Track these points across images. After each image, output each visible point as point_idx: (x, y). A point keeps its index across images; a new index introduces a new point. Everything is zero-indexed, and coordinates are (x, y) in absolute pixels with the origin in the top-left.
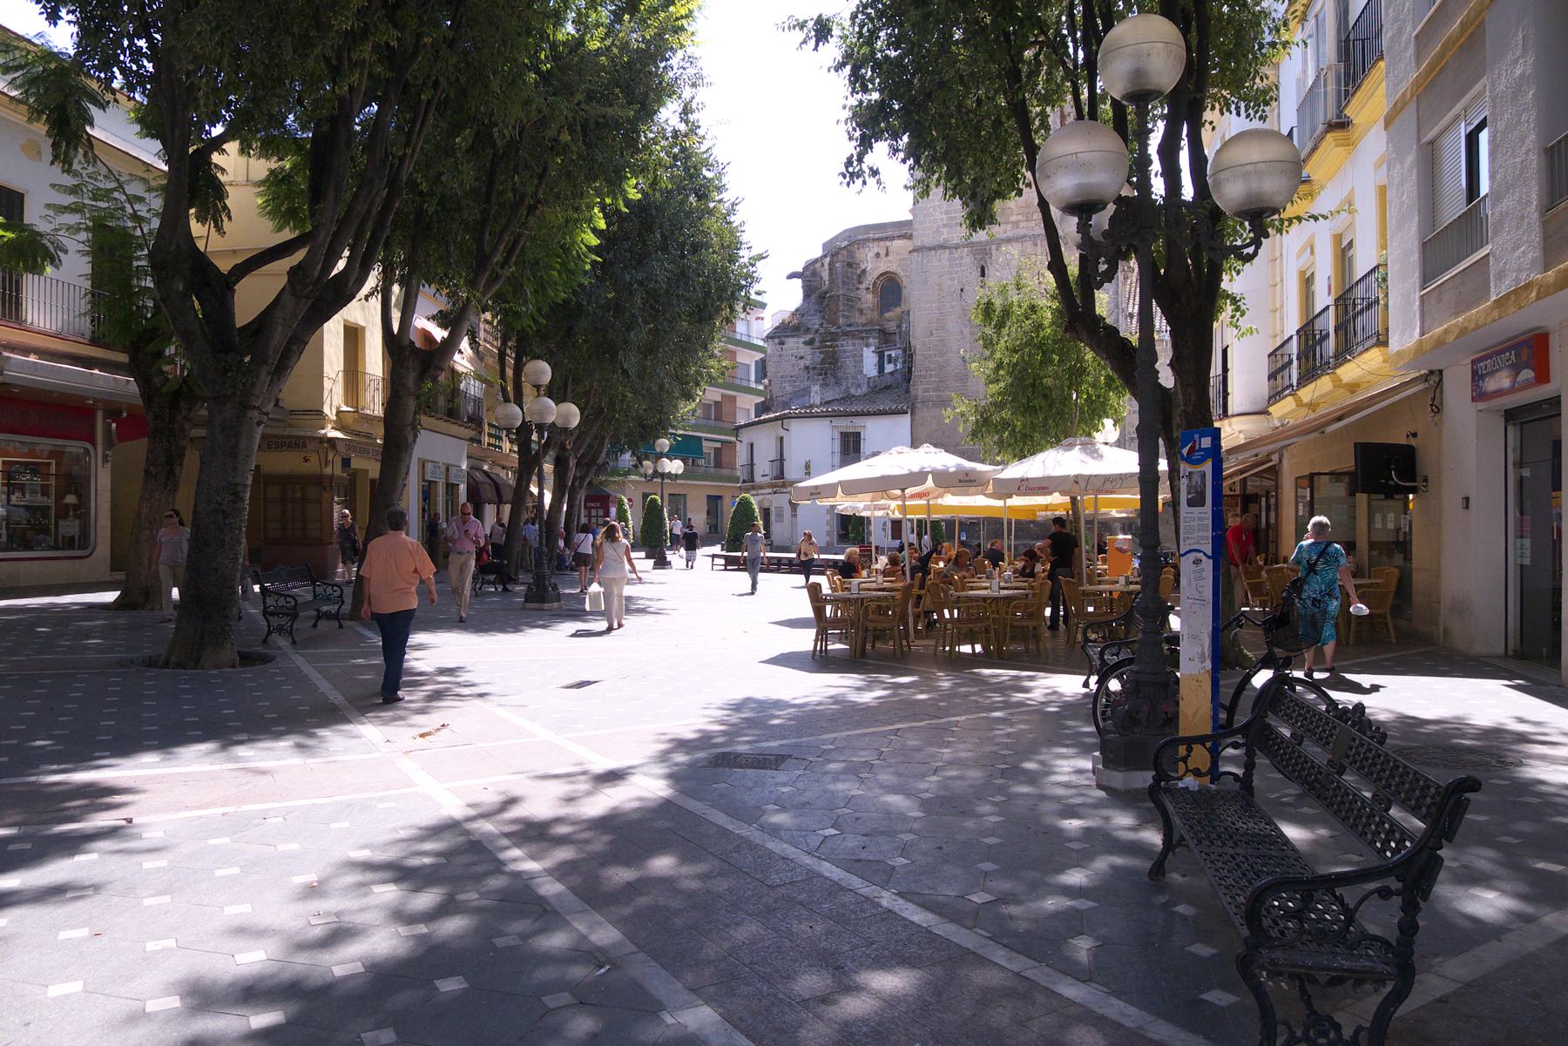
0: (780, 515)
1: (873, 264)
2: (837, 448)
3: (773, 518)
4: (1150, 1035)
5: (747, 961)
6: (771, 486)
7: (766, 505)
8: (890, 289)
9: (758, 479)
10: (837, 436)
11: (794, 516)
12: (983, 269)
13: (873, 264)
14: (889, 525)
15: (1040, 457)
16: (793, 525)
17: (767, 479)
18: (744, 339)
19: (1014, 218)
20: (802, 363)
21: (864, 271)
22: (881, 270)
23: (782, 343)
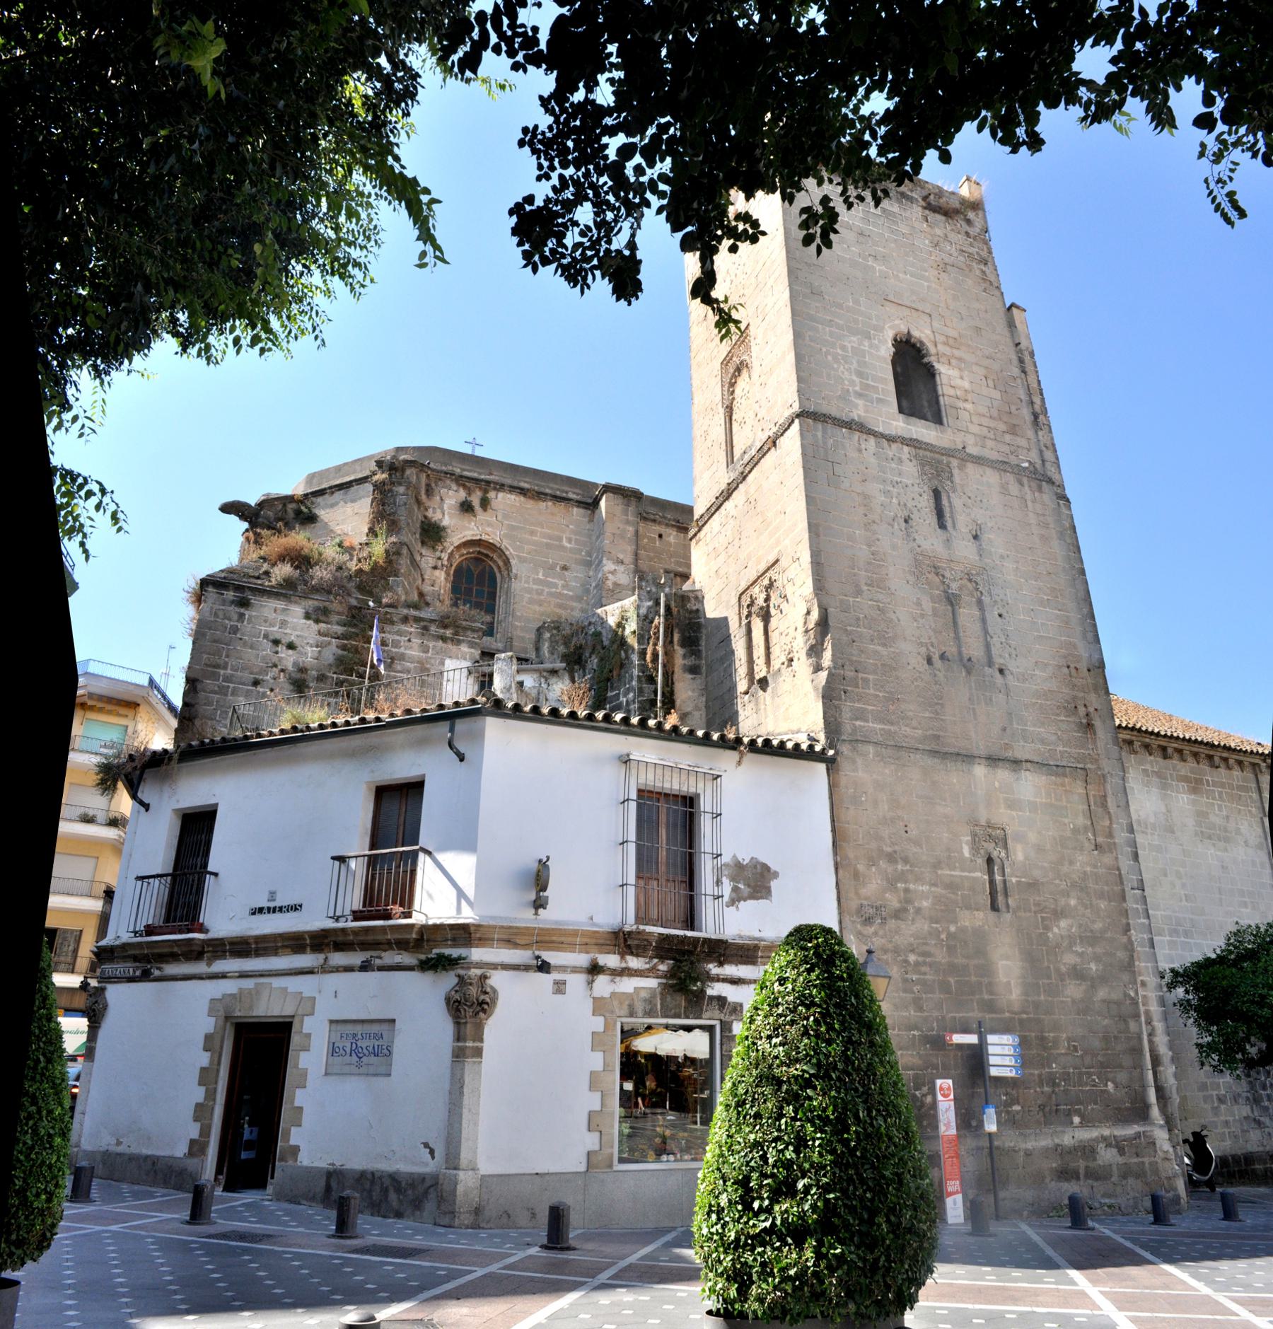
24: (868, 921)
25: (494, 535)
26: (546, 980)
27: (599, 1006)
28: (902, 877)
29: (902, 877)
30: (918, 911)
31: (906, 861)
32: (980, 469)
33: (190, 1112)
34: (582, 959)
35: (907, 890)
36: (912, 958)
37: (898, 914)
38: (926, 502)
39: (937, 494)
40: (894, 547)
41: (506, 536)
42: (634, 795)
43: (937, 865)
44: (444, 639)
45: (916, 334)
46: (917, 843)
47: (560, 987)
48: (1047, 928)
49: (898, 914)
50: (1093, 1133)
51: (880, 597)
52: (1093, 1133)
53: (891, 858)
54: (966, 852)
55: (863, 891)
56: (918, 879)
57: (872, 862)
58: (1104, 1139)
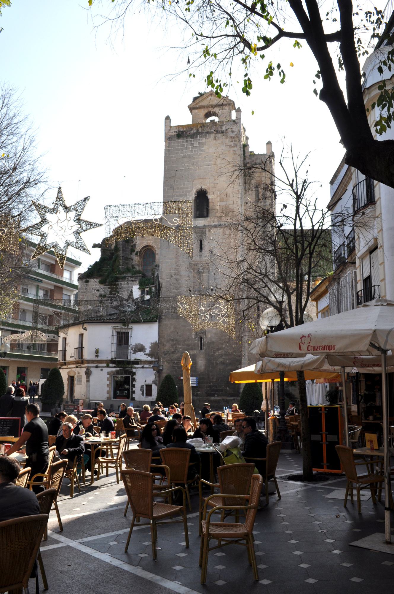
0: (80, 381)
1: (140, 242)
2: (115, 341)
3: (75, 382)
4: (33, 241)
5: (137, 210)
6: (76, 362)
7: (72, 374)
8: (149, 252)
9: (68, 359)
10: (115, 334)
11: (88, 381)
12: (201, 241)
13: (140, 242)
14: (145, 387)
15: (64, 381)
16: (88, 387)
17: (73, 359)
18: (68, 281)
19: (218, 215)
20: (98, 293)
21: (135, 245)
22: (144, 245)
23: (87, 282)
24: (166, 354)
25: (151, 243)
26: (100, 369)
27: (108, 373)
28: (175, 344)
29: (175, 344)
30: (178, 351)
31: (176, 340)
32: (215, 229)
33: (106, 392)
34: (95, 365)
35: (176, 347)
36: (176, 362)
37: (173, 352)
38: (196, 245)
39: (201, 241)
40: (183, 262)
41: (154, 242)
42: (358, 261)
43: (185, 341)
44: (133, 281)
45: (203, 187)
46: (180, 336)
47: (102, 370)
48: (214, 353)
49: (173, 352)
50: (220, 398)
51: (177, 277)
52: (220, 398)
53: (173, 340)
54: (193, 337)
55: (165, 348)
56: (179, 344)
57: (168, 341)
58: (223, 399)
